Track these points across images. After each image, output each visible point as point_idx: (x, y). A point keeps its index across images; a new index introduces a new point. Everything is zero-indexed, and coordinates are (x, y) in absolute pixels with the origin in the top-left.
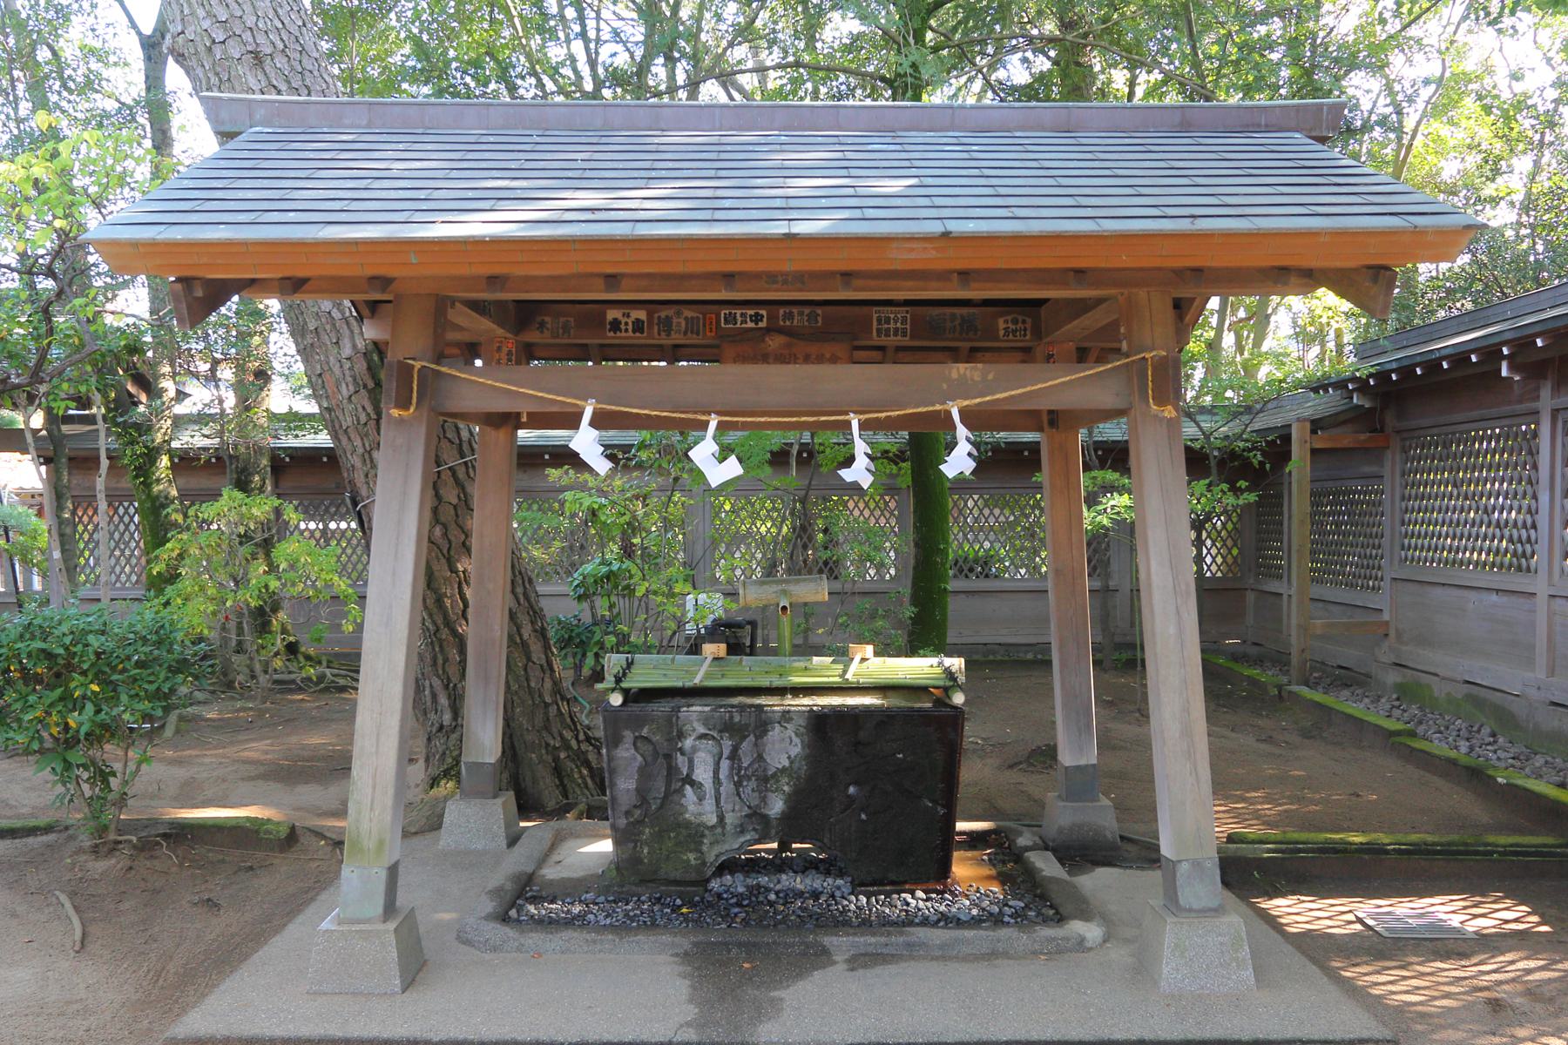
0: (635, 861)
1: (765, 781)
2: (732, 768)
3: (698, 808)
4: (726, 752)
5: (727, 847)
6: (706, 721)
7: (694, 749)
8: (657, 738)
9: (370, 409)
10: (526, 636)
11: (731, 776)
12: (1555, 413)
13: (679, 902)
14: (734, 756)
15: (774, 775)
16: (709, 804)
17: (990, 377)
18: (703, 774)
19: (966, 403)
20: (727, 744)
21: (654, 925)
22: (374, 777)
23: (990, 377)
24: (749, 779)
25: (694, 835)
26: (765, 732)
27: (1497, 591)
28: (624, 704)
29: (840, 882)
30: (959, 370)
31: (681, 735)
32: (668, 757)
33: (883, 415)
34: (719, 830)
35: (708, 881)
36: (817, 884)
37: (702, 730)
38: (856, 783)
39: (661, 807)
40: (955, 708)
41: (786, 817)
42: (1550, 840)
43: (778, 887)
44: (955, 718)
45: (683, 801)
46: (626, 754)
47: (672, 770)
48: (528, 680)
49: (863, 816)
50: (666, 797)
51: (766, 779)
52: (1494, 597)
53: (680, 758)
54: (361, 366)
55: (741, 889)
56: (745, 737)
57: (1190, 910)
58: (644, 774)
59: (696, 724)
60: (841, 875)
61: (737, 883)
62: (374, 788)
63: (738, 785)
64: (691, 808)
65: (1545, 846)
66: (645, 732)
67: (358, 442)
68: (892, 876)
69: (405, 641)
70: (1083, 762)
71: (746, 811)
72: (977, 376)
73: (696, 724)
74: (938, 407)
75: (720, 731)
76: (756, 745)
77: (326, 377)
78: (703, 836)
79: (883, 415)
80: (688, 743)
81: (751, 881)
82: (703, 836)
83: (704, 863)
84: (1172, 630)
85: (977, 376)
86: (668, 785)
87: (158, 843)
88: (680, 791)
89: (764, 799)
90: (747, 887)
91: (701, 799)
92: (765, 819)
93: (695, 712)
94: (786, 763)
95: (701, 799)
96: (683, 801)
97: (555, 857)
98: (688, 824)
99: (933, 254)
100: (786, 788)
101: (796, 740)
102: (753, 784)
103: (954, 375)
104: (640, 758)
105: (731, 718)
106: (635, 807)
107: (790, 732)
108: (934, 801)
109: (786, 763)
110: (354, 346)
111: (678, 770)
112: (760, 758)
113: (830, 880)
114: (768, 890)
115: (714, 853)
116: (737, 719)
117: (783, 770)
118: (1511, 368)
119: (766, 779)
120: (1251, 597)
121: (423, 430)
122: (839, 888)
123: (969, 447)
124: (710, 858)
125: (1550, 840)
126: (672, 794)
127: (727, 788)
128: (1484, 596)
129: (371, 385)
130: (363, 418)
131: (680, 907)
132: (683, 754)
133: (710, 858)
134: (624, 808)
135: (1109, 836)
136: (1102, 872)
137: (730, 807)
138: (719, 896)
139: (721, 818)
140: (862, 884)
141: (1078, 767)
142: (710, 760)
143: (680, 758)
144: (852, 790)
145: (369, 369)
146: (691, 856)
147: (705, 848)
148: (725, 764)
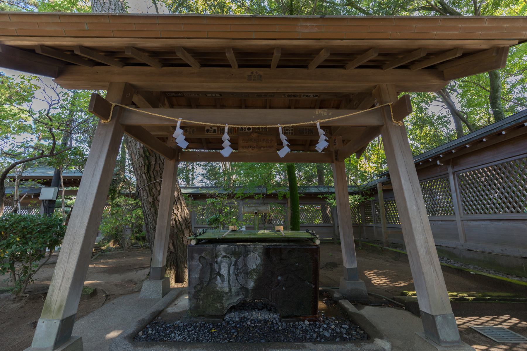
0: (197, 307)
1: (247, 274)
2: (235, 269)
3: (222, 285)
4: (233, 263)
5: (232, 301)
6: (226, 250)
7: (221, 262)
8: (207, 257)
9: (143, 163)
10: (183, 228)
11: (234, 272)
12: (454, 173)
13: (211, 326)
14: (235, 264)
15: (250, 272)
16: (226, 284)
17: (330, 114)
18: (224, 271)
19: (323, 121)
20: (233, 260)
21: (198, 341)
22: (64, 274)
23: (330, 114)
24: (241, 274)
25: (220, 296)
26: (248, 255)
27: (441, 220)
28: (197, 244)
29: (275, 316)
30: (318, 112)
31: (217, 256)
32: (211, 265)
33: (291, 125)
34: (229, 294)
35: (225, 315)
36: (267, 316)
37: (224, 254)
38: (281, 275)
39: (208, 284)
40: (317, 246)
41: (255, 289)
42: (509, 294)
43: (252, 318)
44: (316, 250)
45: (216, 282)
46: (195, 264)
47: (212, 270)
48: (183, 241)
49: (284, 288)
50: (210, 280)
51: (247, 274)
52: (440, 222)
53: (216, 265)
54: (142, 151)
55: (237, 319)
56: (240, 257)
57: (446, 342)
58: (202, 271)
59: (222, 252)
60: (275, 312)
61: (235, 316)
62: (63, 279)
63: (237, 276)
64: (219, 285)
65: (509, 297)
66: (203, 255)
67: (139, 172)
68: (295, 314)
69: (90, 211)
70: (353, 267)
71: (240, 286)
72: (325, 114)
73: (222, 252)
74: (312, 122)
75: (231, 255)
76: (244, 260)
77: (133, 154)
78: (223, 297)
79: (291, 125)
80: (219, 259)
81: (242, 315)
82: (223, 297)
83: (223, 308)
84: (415, 207)
85: (325, 114)
86: (211, 275)
87: (41, 297)
88: (215, 278)
89: (247, 282)
90: (239, 318)
91: (223, 281)
92: (247, 289)
93: (221, 247)
94: (255, 267)
95: (223, 281)
96: (216, 282)
97: (176, 302)
98: (218, 292)
99: (316, 30)
100: (255, 277)
101: (259, 258)
102: (242, 275)
103: (317, 113)
104: (201, 265)
105: (235, 249)
106: (198, 284)
107: (257, 255)
108: (310, 282)
109: (255, 267)
110: (140, 146)
111: (215, 269)
112: (245, 265)
113: (271, 314)
114: (248, 319)
115: (227, 303)
116: (237, 250)
117: (254, 270)
118: (440, 162)
119: (247, 274)
120: (364, 228)
121: (112, 129)
122: (275, 318)
123: (325, 137)
124: (226, 306)
125: (509, 294)
126: (212, 279)
127: (233, 277)
128: (437, 222)
129: (144, 156)
130: (141, 165)
131: (211, 329)
132: (217, 263)
133: (226, 306)
134: (194, 285)
135: (364, 293)
136: (367, 308)
137: (233, 285)
138: (228, 323)
139: (230, 289)
140: (284, 317)
141: (351, 269)
142: (227, 266)
143: (216, 265)
144: (279, 278)
145: (144, 151)
146: (219, 305)
147: (224, 302)
148: (232, 268)
